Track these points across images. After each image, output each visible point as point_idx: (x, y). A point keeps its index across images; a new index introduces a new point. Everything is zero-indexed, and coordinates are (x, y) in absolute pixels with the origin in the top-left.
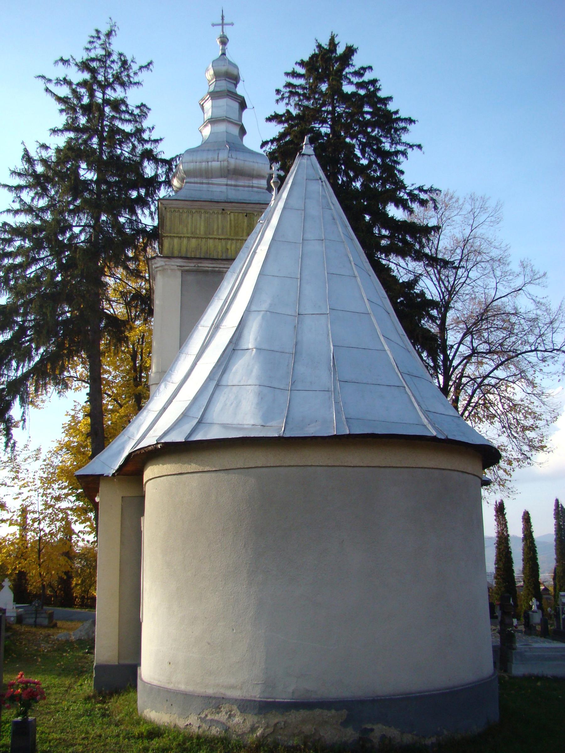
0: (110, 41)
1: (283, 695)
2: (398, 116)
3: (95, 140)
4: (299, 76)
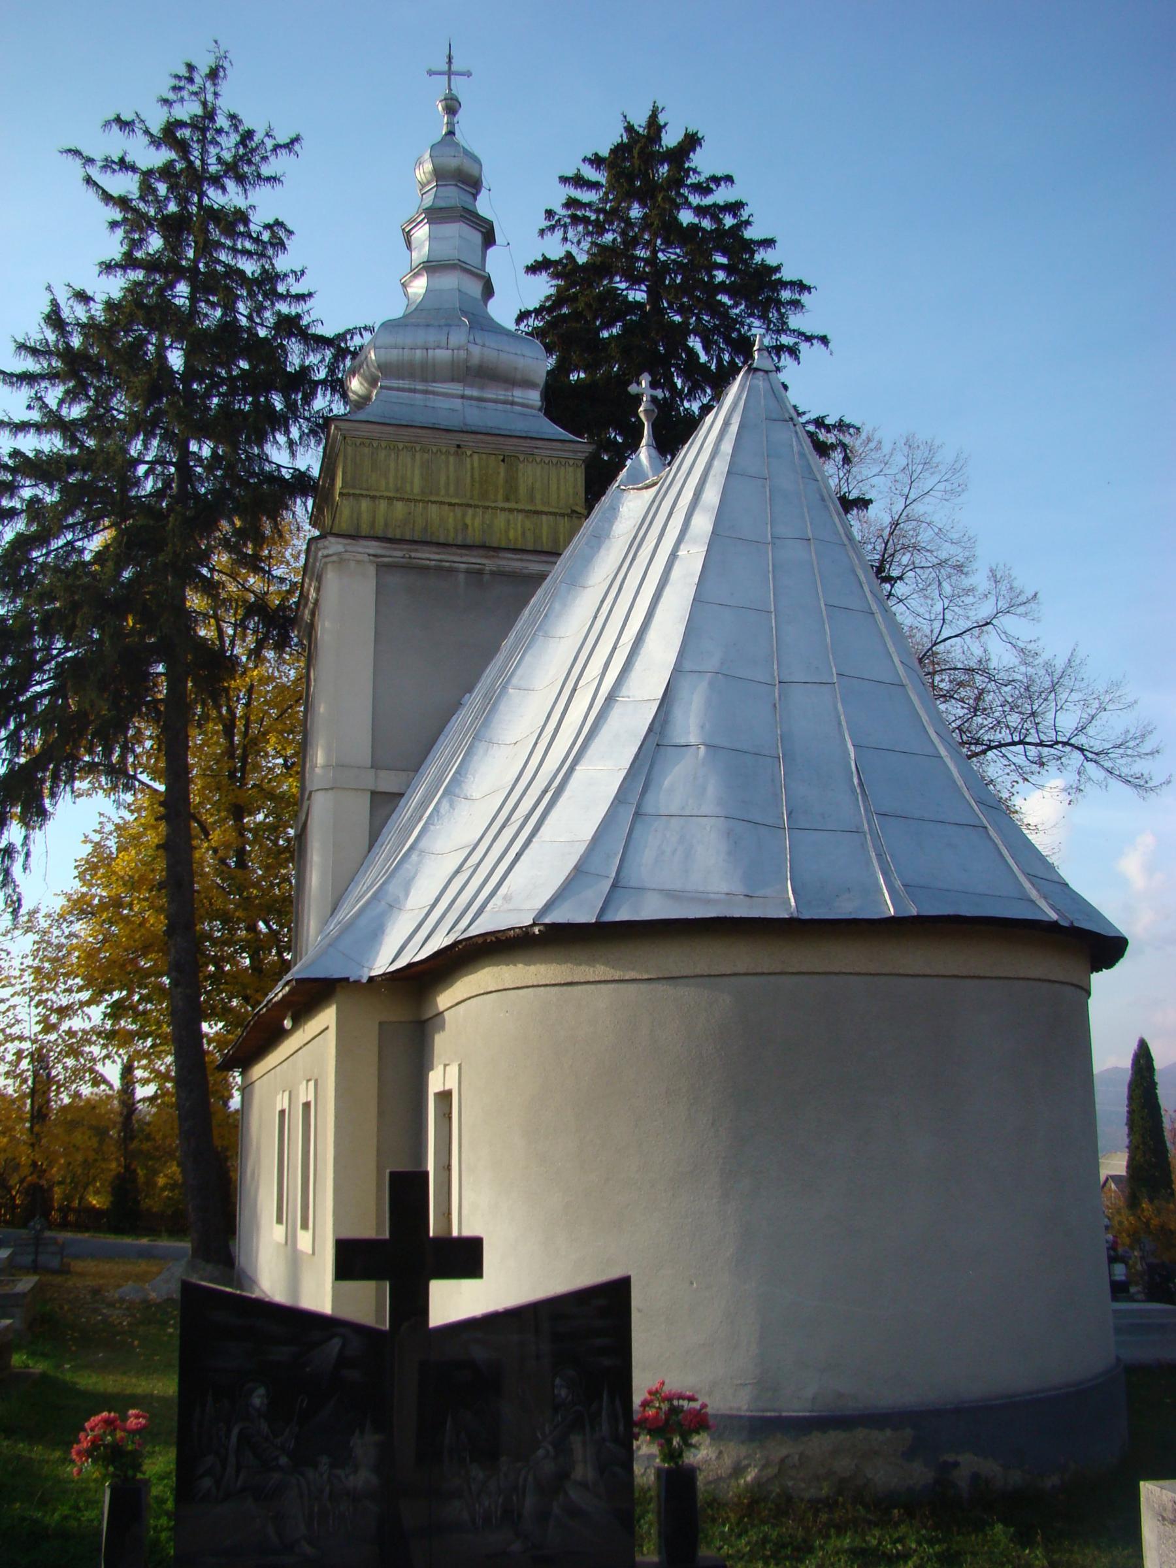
0: (218, 89)
1: (795, 1406)
2: (778, 276)
3: (183, 288)
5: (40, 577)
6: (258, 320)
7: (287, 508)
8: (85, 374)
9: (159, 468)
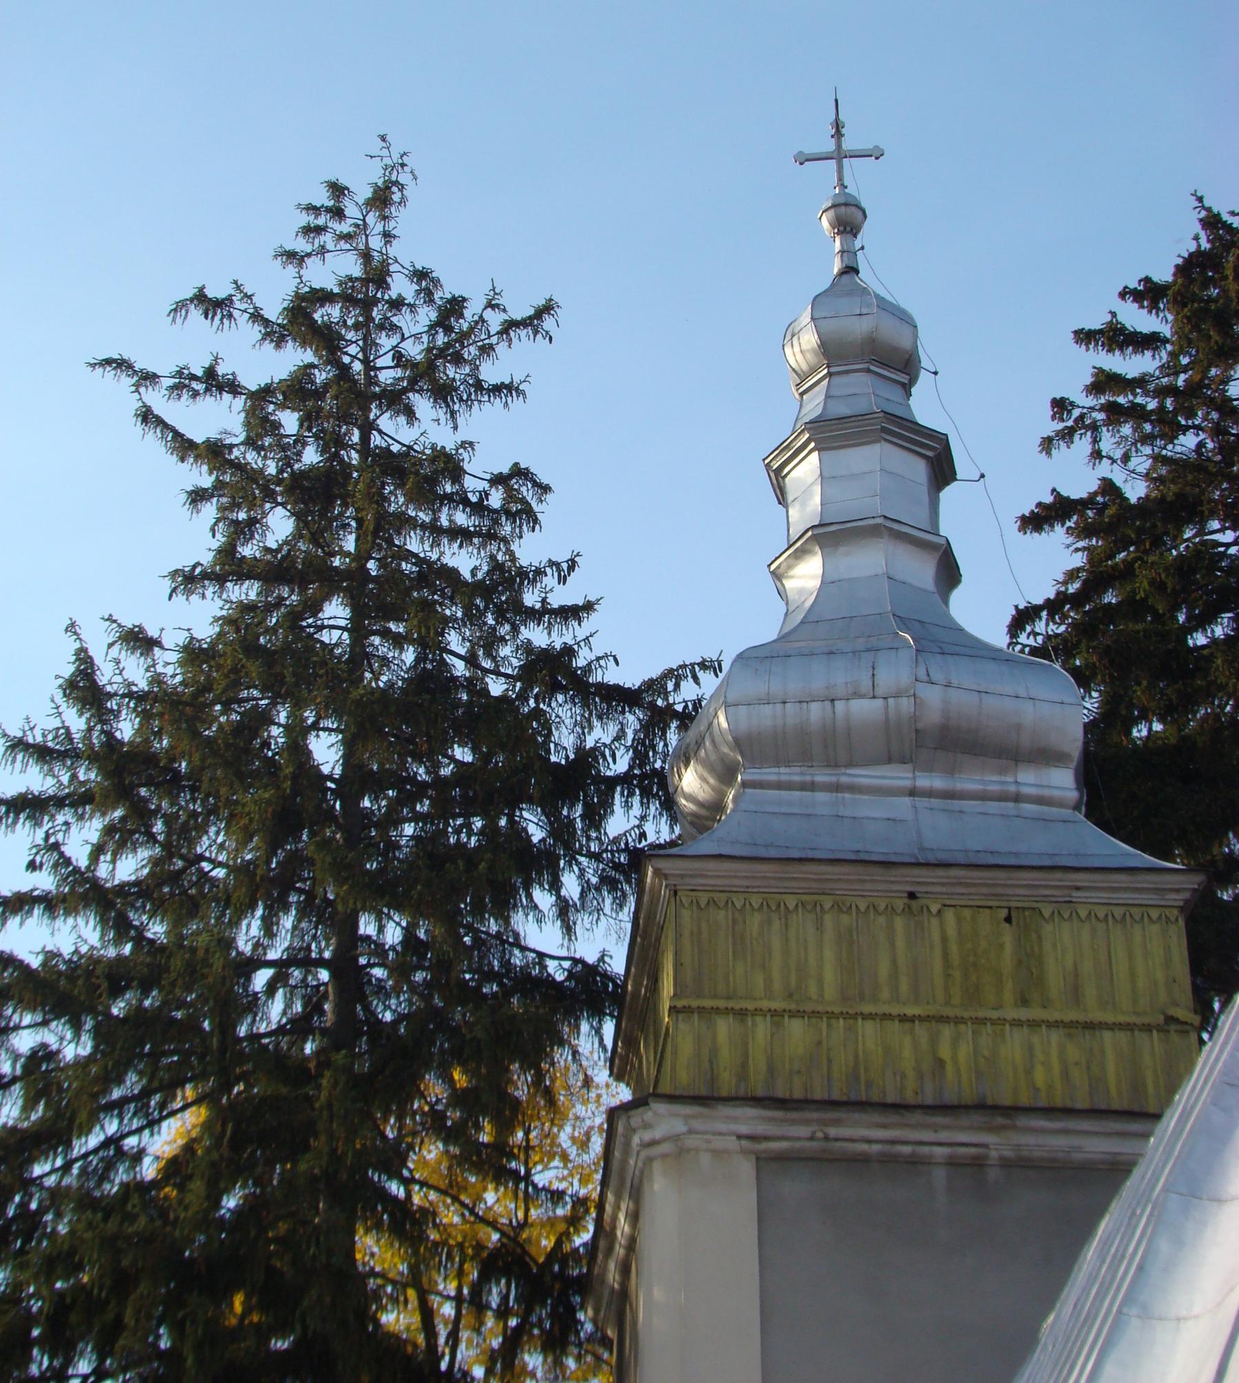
3: (336, 611)
4: (1147, 342)
5: (49, 1217)
6: (487, 664)
7: (562, 1042)
8: (143, 792)
9: (297, 974)
